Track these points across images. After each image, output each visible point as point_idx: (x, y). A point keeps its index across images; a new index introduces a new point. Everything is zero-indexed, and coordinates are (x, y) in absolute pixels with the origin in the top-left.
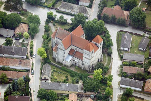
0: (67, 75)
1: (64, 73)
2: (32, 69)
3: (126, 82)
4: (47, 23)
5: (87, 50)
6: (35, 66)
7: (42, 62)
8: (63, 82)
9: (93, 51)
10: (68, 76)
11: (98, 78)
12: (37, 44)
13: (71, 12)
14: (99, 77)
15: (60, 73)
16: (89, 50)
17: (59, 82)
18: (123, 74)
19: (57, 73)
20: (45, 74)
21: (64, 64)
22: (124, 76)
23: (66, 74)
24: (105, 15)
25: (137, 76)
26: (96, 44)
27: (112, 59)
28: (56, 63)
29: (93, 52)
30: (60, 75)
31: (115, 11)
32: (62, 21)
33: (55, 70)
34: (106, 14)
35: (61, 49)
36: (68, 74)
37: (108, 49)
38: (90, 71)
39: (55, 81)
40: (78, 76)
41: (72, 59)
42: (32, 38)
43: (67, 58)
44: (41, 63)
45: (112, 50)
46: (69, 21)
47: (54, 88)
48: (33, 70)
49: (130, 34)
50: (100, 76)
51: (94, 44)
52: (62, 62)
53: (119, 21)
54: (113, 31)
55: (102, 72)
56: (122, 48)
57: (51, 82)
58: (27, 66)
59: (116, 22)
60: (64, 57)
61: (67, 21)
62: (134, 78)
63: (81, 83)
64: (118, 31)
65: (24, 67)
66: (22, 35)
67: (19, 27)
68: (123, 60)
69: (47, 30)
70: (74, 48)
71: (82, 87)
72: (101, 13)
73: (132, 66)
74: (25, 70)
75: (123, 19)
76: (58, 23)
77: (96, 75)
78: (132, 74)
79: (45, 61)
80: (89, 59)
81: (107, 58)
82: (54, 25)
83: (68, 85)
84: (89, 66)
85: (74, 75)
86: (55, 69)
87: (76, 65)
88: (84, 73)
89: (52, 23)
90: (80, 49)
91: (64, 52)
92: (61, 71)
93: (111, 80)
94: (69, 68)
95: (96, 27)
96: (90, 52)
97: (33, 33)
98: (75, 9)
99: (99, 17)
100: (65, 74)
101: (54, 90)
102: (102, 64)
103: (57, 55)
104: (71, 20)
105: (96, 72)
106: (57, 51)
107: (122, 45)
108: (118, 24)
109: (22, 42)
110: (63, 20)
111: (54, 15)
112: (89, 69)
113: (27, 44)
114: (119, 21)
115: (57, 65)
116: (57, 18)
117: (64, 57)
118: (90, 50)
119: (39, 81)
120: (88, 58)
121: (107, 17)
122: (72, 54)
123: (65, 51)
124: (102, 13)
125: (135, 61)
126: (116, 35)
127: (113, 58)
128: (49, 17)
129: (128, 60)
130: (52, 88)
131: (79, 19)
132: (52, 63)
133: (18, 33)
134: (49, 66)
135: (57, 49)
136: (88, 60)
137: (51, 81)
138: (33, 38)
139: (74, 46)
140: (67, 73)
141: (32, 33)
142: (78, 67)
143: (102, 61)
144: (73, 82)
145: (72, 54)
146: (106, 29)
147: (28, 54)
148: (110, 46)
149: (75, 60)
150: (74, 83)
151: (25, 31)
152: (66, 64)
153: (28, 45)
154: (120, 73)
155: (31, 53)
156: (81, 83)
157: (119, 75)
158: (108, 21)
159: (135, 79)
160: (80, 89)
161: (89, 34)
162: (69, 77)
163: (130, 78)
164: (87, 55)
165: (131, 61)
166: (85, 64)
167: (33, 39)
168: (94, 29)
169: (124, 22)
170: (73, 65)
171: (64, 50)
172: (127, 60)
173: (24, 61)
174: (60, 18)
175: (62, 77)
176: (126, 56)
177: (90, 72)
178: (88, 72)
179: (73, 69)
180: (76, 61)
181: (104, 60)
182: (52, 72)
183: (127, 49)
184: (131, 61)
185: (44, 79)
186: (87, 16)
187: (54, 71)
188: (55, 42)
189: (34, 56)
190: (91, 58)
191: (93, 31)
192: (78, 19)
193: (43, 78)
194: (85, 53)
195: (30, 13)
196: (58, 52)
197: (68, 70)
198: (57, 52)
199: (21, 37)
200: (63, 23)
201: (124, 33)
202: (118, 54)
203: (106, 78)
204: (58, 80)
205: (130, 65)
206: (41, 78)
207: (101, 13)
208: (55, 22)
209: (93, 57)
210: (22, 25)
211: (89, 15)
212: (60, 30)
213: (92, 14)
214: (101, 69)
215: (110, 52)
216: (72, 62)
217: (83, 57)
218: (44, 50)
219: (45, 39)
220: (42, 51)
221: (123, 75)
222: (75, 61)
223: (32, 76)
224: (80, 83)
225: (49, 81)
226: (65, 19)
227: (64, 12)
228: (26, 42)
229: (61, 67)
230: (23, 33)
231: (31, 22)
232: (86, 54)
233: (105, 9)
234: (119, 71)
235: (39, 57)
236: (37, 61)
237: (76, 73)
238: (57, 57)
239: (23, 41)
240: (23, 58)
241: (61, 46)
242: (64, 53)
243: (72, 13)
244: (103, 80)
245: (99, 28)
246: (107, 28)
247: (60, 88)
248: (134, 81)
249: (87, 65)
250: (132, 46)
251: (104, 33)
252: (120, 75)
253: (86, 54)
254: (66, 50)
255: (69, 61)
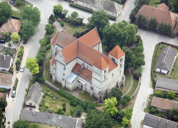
0: (64, 103)
1: (62, 99)
2: (15, 89)
3: (151, 121)
4: (51, 21)
5: (97, 67)
6: (20, 85)
7: (32, 79)
8: (57, 113)
9: (107, 69)
10: (67, 105)
11: (109, 111)
12: (30, 52)
13: (92, 8)
14: (111, 110)
15: (54, 98)
16: (100, 68)
17: (51, 112)
18: (151, 110)
19: (51, 99)
20: (30, 98)
21: (63, 85)
22: (151, 113)
23: (64, 101)
24: (140, 17)
25: (171, 114)
26: (113, 60)
27: (140, 84)
28: (53, 83)
29: (107, 71)
30: (54, 101)
31: (158, 11)
32: (74, 19)
33: (49, 93)
34: (143, 15)
35: (60, 63)
36: (66, 102)
37: (136, 68)
38: (101, 99)
39: (45, 110)
40: (82, 105)
41: (76, 79)
42: (24, 42)
43: (69, 77)
44: (30, 82)
45: (141, 71)
46: (86, 22)
47: (40, 121)
48: (15, 90)
49: (174, 49)
50: (113, 109)
51: (111, 58)
52: (61, 81)
53: (162, 28)
54: (149, 43)
55: (117, 102)
56: (158, 70)
57: (39, 111)
58: (6, 83)
59: (157, 28)
60: (64, 74)
61: (82, 21)
62: (167, 117)
63: (83, 117)
64: (158, 42)
65: (2, 85)
66: (9, 37)
67: (7, 24)
68: (155, 88)
69: (50, 31)
70: (80, 62)
71: (83, 123)
72: (136, 13)
73: (168, 98)
74: (3, 89)
75: (167, 25)
76: (68, 22)
77: (106, 106)
78: (165, 110)
79: (37, 78)
80: (100, 81)
81: (132, 82)
82: (62, 25)
83: (61, 118)
84: (100, 93)
85: (75, 103)
86: (48, 91)
87: (81, 89)
88: (91, 102)
89: (59, 21)
90: (89, 64)
91: (64, 67)
92: (58, 96)
93: (129, 117)
94: (71, 93)
95: (121, 34)
96: (101, 70)
97: (26, 35)
98: (98, 3)
99: (133, 19)
100: (62, 100)
101: (40, 123)
102: (118, 91)
103: (54, 71)
104: (88, 19)
105: (108, 102)
106: (54, 65)
107: (158, 64)
108: (159, 31)
109: (8, 47)
110: (77, 19)
111: (63, 10)
112: (101, 97)
113: (14, 51)
114: (162, 28)
115: (52, 86)
116: (68, 14)
117: (64, 74)
118: (101, 68)
119: (22, 108)
120: (99, 80)
121: (144, 20)
122: (78, 71)
123: (65, 66)
124: (137, 14)
125: (174, 90)
126: (153, 49)
127: (141, 83)
128: (56, 12)
129: (163, 88)
130: (38, 121)
131: (98, 19)
132: (47, 82)
133: (4, 32)
134: (40, 86)
135: (55, 61)
136: (99, 83)
137: (39, 109)
138: (25, 42)
139: (81, 60)
140: (66, 100)
141: (25, 35)
142: (85, 92)
143: (124, 86)
144: (71, 115)
145: (78, 71)
146: (139, 39)
147: (13, 65)
148: (140, 65)
149: (80, 81)
150: (74, 116)
151: (14, 31)
152: (67, 86)
153: (16, 52)
154: (147, 107)
155: (18, 64)
156: (83, 117)
157: (145, 110)
158: (146, 25)
159: (168, 118)
160: (79, 126)
161: (109, 43)
162: (68, 106)
163: (160, 116)
164: (97, 74)
165: (168, 90)
166: (95, 88)
167: (26, 44)
168: (117, 35)
169: (169, 30)
170: (78, 88)
171: (64, 65)
172: (162, 88)
173: (2, 75)
174: (72, 15)
175: (56, 105)
176: (161, 83)
177: (101, 101)
178: (99, 101)
179: (76, 95)
180: (82, 82)
181: (128, 84)
182: (43, 97)
183: (166, 72)
184: (168, 90)
185: (29, 105)
186: (115, 15)
187: (46, 94)
188: (55, 51)
189: (21, 70)
190: (103, 79)
191: (115, 40)
192: (96, 20)
193: (28, 103)
194: (95, 72)
195: (30, 4)
196: (56, 66)
197: (68, 96)
198: (55, 67)
199: (8, 39)
200: (76, 23)
201: (166, 46)
202: (150, 77)
203: (123, 112)
204: (49, 109)
205: (165, 95)
206: (25, 104)
207: (135, 13)
208: (65, 21)
209: (107, 78)
210: (11, 21)
211: (117, 15)
212: (62, 33)
213: (123, 13)
214: (115, 99)
215: (137, 74)
216: (77, 84)
217: (92, 78)
218: (36, 62)
219: (43, 45)
220: (33, 63)
221: (151, 110)
222: (80, 82)
223: (12, 99)
224: (83, 116)
225: (37, 110)
226: (79, 17)
227: (81, 7)
228: (13, 47)
229: (59, 90)
230: (10, 33)
231: (24, 18)
232: (96, 73)
233: (144, 6)
234: (147, 103)
235: (27, 71)
236: (24, 78)
237: (79, 100)
238: (54, 74)
239: (10, 45)
240: (4, 70)
241: (60, 58)
242: (65, 69)
243: (92, 10)
244: (118, 115)
245: (125, 36)
246: (141, 37)
247: (48, 121)
248: (165, 122)
249: (97, 91)
250: (174, 68)
251: (133, 45)
252: (147, 111)
253: (96, 73)
254: (67, 64)
255: (71, 81)
